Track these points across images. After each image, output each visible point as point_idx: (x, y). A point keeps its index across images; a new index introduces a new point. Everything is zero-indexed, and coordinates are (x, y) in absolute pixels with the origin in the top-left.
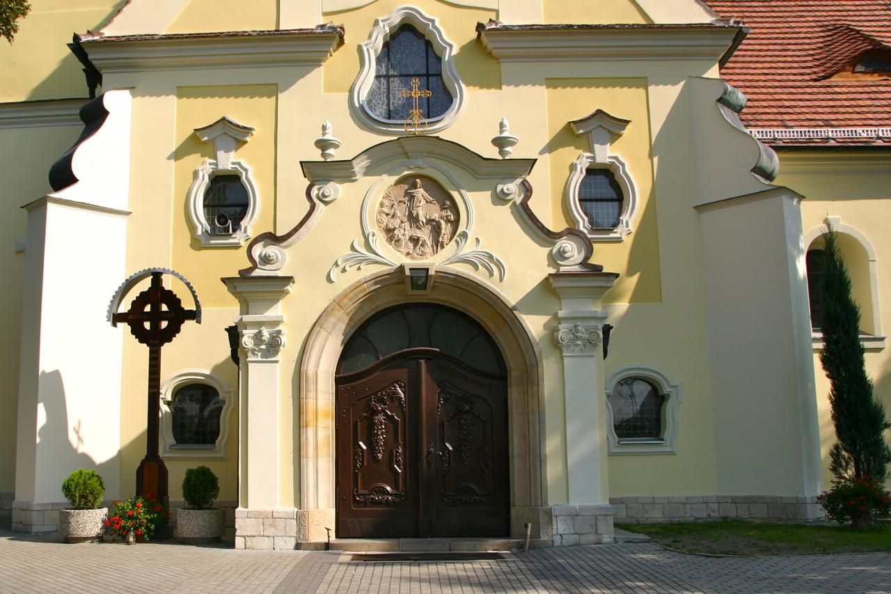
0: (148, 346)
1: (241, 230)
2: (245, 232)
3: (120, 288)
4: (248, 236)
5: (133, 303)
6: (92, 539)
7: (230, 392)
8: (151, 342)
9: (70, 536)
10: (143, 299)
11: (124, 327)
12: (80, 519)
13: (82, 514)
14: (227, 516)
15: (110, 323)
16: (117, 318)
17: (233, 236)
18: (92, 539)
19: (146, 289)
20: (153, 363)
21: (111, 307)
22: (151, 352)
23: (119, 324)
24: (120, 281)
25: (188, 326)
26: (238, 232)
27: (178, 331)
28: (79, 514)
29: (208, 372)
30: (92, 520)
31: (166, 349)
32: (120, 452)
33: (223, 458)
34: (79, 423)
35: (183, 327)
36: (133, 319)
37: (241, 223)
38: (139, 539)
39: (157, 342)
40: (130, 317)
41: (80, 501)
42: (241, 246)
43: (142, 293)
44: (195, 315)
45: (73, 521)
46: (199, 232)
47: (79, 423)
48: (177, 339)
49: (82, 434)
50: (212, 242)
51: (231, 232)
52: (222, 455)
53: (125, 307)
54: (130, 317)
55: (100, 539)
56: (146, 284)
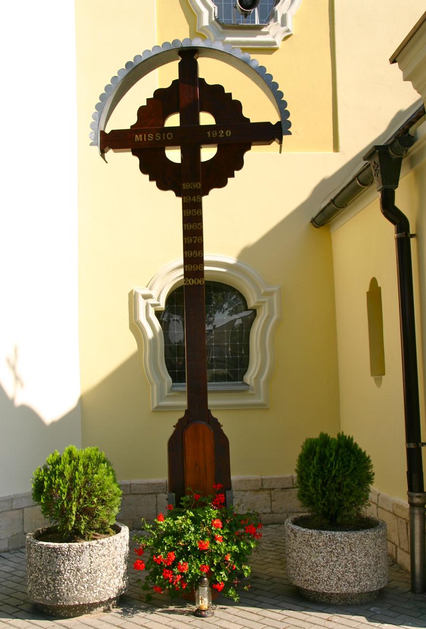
0: (178, 195)
1: (276, 20)
2: (284, 23)
3: (114, 79)
4: (288, 31)
5: (142, 111)
6: (106, 605)
7: (270, 294)
8: (185, 186)
9: (60, 603)
10: (162, 102)
11: (126, 162)
12: (84, 563)
13: (87, 552)
14: (102, 464)
15: (97, 149)
16: (111, 141)
17: (264, 30)
18: (106, 605)
19: (167, 84)
20: (191, 227)
21: (97, 117)
22: (185, 206)
23: (110, 154)
24: (116, 66)
25: (256, 156)
26: (272, 23)
27: (239, 165)
28: (80, 552)
29: (232, 260)
30: (103, 562)
31: (213, 202)
32: (81, 400)
33: (264, 405)
34: (16, 351)
35: (247, 156)
36: (142, 142)
37: (277, 8)
38: (219, 598)
39: (198, 185)
40: (138, 138)
41: (78, 520)
42: (276, 49)
43: (159, 93)
44: (272, 133)
45: (66, 568)
46: (206, 22)
47: (16, 351)
48: (237, 181)
49: (20, 370)
50: (228, 39)
51: (257, 22)
52: (261, 400)
53: (125, 117)
54: (138, 138)
55: (125, 601)
56: (166, 75)
